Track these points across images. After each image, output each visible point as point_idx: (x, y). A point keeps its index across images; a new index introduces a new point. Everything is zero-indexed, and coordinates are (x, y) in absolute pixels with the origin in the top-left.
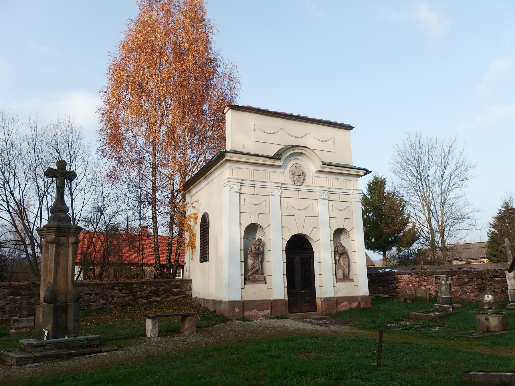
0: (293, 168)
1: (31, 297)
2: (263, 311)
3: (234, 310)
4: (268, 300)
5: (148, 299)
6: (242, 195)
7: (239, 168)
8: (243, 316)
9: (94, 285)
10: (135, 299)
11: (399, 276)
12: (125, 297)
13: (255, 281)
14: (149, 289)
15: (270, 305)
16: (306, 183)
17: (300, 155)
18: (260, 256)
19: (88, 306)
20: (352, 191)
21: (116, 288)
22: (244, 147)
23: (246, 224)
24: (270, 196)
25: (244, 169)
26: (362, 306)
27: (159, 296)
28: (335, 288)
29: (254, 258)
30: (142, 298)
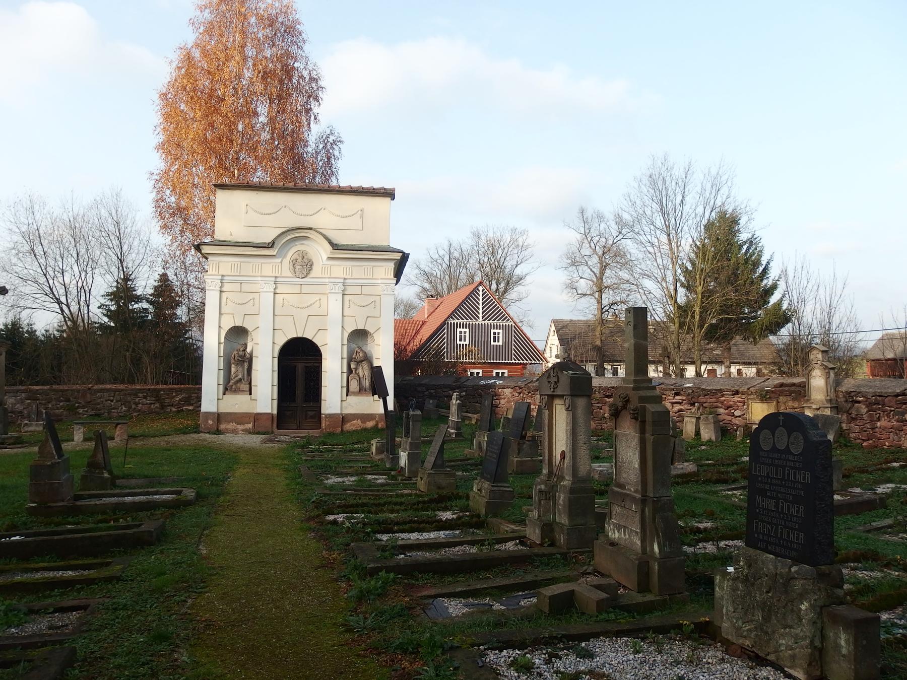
0: (296, 256)
1: (49, 402)
2: (244, 424)
3: (208, 422)
4: (250, 413)
5: (180, 407)
6: (345, 296)
7: (375, 266)
8: (218, 429)
9: (115, 391)
10: (163, 407)
11: (500, 390)
12: (150, 404)
13: (237, 391)
14: (180, 397)
15: (253, 419)
16: (313, 274)
17: (306, 239)
18: (246, 364)
19: (109, 413)
20: (380, 281)
21: (140, 395)
22: (231, 235)
23: (350, 329)
24: (329, 295)
25: (250, 262)
26: (380, 426)
27: (192, 405)
28: (344, 403)
29: (237, 365)
30: (172, 406)
